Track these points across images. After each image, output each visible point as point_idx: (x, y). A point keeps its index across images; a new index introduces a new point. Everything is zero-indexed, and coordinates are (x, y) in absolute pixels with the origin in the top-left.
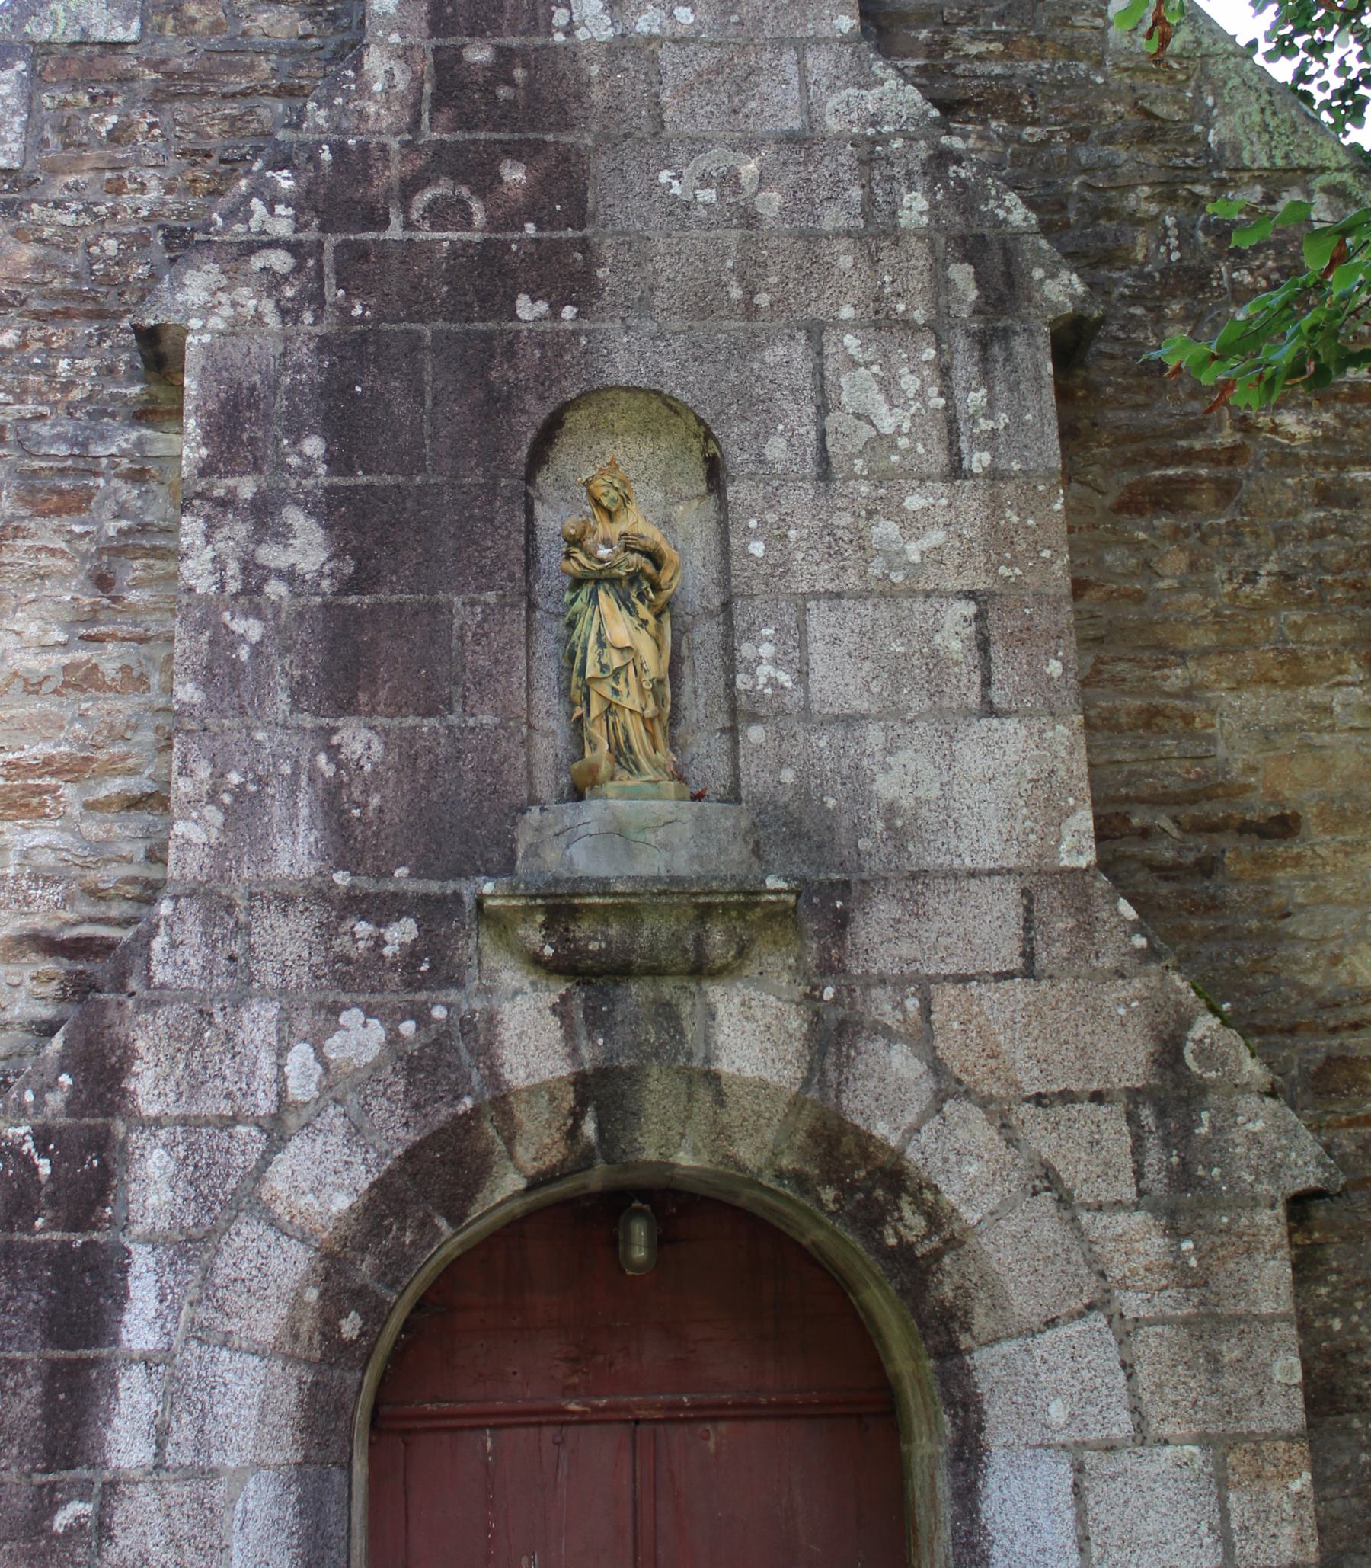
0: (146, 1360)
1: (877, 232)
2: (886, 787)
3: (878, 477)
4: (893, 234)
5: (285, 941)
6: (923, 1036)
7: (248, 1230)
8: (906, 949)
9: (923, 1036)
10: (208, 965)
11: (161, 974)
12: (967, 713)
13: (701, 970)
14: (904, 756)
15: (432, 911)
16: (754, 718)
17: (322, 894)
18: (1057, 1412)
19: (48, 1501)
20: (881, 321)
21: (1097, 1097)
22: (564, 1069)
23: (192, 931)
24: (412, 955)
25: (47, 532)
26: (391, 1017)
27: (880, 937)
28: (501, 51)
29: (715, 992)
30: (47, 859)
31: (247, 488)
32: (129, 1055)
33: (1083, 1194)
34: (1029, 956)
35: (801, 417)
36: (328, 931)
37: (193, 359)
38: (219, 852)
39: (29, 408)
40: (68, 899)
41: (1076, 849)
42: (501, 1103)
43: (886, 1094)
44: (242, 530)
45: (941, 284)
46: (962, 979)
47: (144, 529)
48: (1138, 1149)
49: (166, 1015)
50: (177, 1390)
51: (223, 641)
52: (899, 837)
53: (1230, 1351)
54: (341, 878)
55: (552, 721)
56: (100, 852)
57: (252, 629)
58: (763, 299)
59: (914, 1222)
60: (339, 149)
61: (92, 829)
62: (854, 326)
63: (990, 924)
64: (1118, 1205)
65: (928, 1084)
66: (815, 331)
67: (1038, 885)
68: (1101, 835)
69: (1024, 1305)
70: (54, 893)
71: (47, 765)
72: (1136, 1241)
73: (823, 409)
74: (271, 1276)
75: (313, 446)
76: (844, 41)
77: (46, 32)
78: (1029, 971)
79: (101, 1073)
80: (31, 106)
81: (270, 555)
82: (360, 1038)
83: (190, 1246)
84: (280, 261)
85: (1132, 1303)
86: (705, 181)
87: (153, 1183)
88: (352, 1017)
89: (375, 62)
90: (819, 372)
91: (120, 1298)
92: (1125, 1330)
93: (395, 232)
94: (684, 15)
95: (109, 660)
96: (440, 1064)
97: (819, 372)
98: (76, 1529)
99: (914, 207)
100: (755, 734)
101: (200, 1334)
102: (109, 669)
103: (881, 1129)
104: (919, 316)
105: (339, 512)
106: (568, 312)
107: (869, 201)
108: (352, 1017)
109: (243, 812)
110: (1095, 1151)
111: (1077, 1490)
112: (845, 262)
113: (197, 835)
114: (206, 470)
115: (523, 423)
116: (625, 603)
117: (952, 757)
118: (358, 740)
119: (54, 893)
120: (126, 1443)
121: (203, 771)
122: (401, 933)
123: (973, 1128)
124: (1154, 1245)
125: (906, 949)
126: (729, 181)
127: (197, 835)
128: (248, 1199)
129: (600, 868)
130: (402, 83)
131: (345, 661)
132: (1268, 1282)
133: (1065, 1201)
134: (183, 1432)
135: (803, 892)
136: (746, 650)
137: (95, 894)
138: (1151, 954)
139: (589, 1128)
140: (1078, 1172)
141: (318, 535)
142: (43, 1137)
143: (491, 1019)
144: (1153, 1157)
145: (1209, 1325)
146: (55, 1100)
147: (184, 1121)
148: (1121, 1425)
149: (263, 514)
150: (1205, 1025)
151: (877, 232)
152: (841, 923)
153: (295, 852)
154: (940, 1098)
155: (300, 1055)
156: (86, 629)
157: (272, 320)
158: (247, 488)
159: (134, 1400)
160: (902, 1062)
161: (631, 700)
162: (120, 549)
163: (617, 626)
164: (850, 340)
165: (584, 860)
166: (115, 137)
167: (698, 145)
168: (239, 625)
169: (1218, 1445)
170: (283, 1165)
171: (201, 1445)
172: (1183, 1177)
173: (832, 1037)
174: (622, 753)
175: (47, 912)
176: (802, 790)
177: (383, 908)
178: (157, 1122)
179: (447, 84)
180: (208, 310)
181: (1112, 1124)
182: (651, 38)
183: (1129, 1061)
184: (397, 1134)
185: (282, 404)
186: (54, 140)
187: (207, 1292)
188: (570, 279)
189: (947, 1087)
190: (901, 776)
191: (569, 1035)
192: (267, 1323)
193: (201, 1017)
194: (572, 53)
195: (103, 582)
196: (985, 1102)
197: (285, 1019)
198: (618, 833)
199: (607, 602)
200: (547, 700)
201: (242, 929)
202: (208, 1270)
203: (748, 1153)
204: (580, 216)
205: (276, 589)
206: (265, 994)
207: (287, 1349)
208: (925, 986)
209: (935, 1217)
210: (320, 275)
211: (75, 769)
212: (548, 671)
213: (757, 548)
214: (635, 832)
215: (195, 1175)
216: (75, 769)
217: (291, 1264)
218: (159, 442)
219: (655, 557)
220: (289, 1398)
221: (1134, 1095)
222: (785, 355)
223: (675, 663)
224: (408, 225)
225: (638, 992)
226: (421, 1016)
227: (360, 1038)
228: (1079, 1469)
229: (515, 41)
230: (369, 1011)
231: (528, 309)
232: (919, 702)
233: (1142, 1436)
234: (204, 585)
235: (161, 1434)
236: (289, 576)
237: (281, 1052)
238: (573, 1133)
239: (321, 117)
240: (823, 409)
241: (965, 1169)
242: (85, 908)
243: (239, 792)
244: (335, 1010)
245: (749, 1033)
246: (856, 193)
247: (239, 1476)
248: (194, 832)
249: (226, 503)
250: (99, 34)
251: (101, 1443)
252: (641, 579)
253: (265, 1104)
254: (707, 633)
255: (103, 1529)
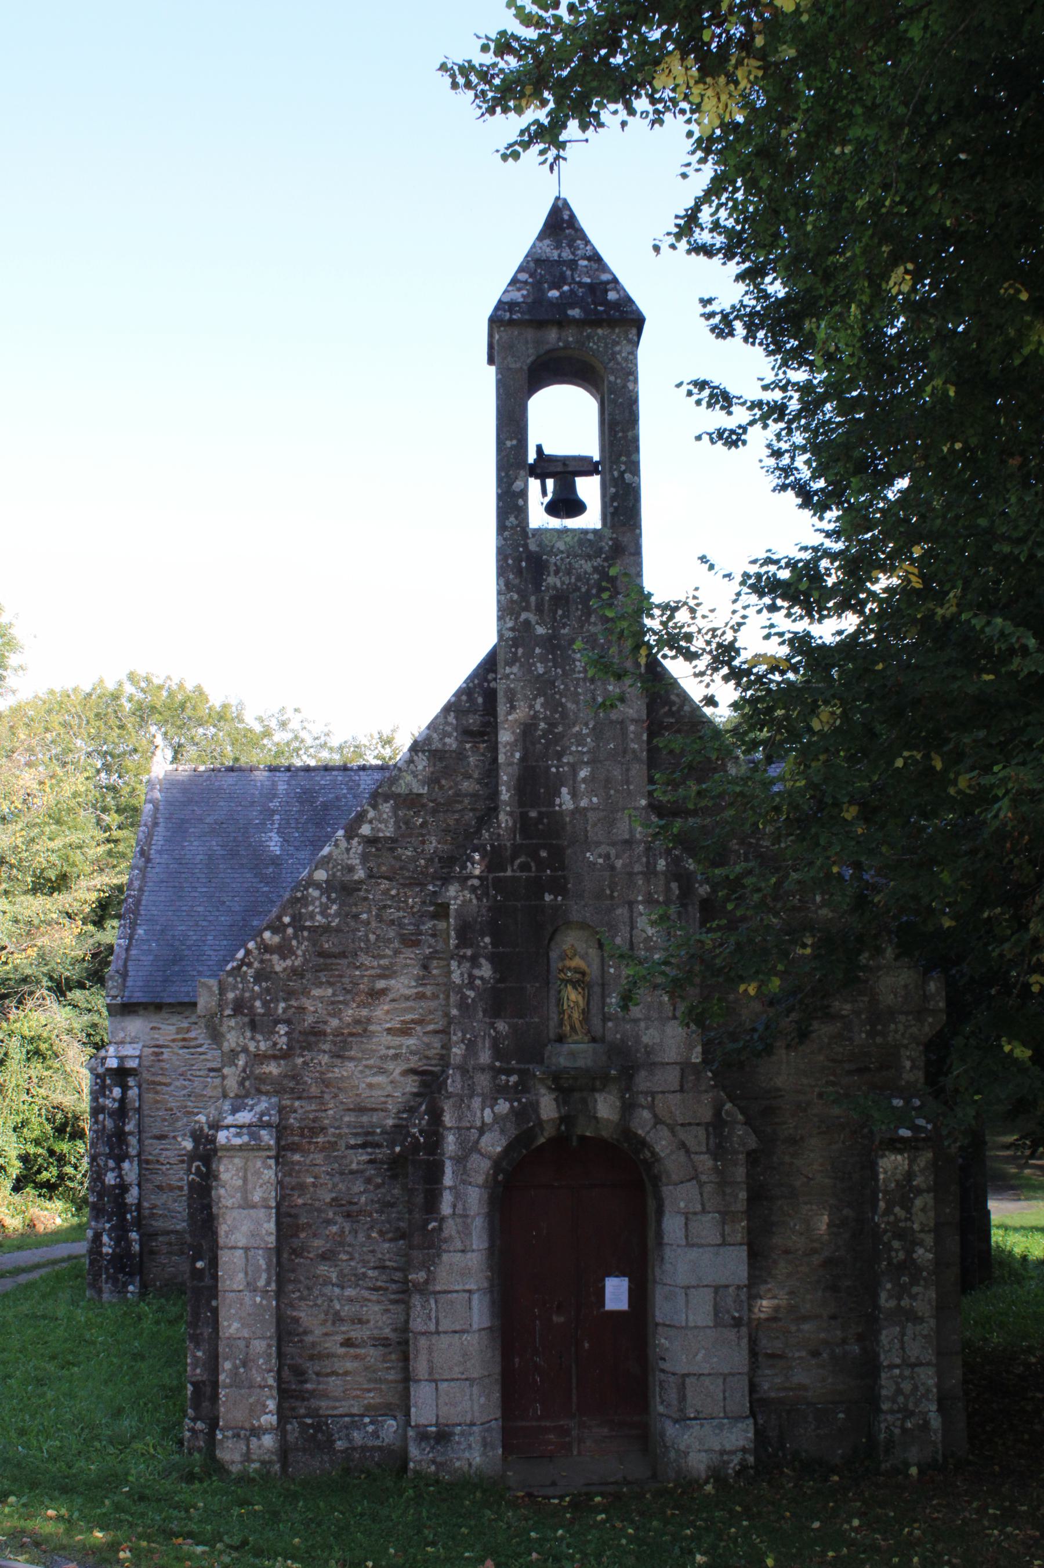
0: (450, 1188)
1: (650, 872)
2: (645, 1039)
3: (647, 949)
4: (655, 873)
5: (483, 1081)
6: (652, 1107)
7: (475, 1156)
8: (648, 1084)
9: (652, 1107)
10: (463, 1087)
11: (450, 1089)
12: (669, 1019)
13: (594, 1090)
14: (651, 1030)
15: (523, 1073)
16: (610, 1020)
17: (492, 1068)
18: (682, 1205)
19: (427, 1222)
20: (650, 901)
21: (698, 1124)
22: (556, 1115)
23: (458, 1078)
24: (516, 1084)
25: (408, 953)
26: (511, 1102)
27: (643, 1081)
28: (540, 813)
29: (597, 1095)
30: (414, 1048)
31: (469, 952)
32: (443, 1111)
33: (693, 1149)
34: (682, 1086)
35: (625, 931)
36: (494, 1078)
37: (452, 913)
38: (464, 1057)
39: (401, 914)
40: (420, 1059)
41: (696, 1058)
42: (540, 1123)
43: (642, 1121)
44: (468, 965)
45: (668, 890)
46: (663, 1092)
47: (436, 952)
48: (708, 1138)
49: (452, 1100)
50: (458, 1196)
51: (464, 997)
52: (648, 1053)
53: (728, 1190)
54: (497, 1064)
55: (554, 1016)
56: (428, 1046)
57: (471, 994)
58: (616, 894)
59: (648, 1154)
60: (492, 846)
61: (426, 1039)
62: (641, 902)
63: (671, 1078)
64: (701, 1153)
65: (652, 1122)
66: (631, 904)
67: (685, 1066)
68: (704, 1053)
69: (674, 1177)
70: (416, 1058)
71: (413, 1021)
72: (705, 1162)
73: (632, 929)
74: (480, 1167)
75: (487, 940)
76: (643, 808)
77: (399, 791)
78: (682, 1090)
79: (436, 1115)
80: (396, 815)
81: (477, 972)
82: (503, 1107)
83: (460, 1161)
84: (476, 882)
85: (704, 1178)
86: (600, 856)
87: (451, 1143)
88: (501, 1101)
89: (502, 817)
90: (631, 917)
91: (443, 1173)
92: (701, 1185)
93: (509, 873)
94: (595, 800)
95: (428, 990)
96: (525, 1114)
97: (631, 917)
98: (434, 1229)
99: (661, 864)
100: (610, 1024)
101: (463, 1182)
102: (429, 994)
103: (640, 1132)
104: (661, 899)
105: (493, 959)
106: (560, 898)
107: (648, 862)
108: (501, 1101)
109: (471, 1047)
110: (695, 1139)
111: (686, 1224)
112: (640, 882)
113: (458, 1052)
114: (457, 947)
115: (544, 928)
116: (575, 988)
117: (664, 1031)
118: (502, 1026)
119: (416, 1058)
120: (446, 1209)
121: (460, 1034)
122: (514, 1079)
123: (665, 1132)
124: (710, 1163)
125: (648, 1084)
126: (607, 857)
127: (458, 1052)
128: (475, 1148)
129: (568, 1064)
130: (510, 824)
131: (498, 1001)
132: (740, 1173)
133: (688, 1152)
134: (460, 1206)
135: (624, 1065)
136: (608, 1000)
137: (427, 1058)
138: (714, 1087)
139: (563, 1128)
140: (691, 1142)
141: (489, 966)
142: (421, 1132)
143: (538, 1102)
144: (711, 1141)
145: (723, 1181)
146: (424, 1122)
147: (458, 1128)
148: (698, 1208)
149: (474, 961)
150: (728, 1106)
151: (650, 872)
152: (631, 1077)
153: (485, 1057)
154: (656, 1124)
155: (487, 1111)
156: (421, 981)
157: (475, 901)
158: (469, 952)
159: (447, 1198)
160: (646, 1114)
161: (576, 1015)
162: (429, 958)
163: (573, 996)
164: (641, 907)
165: (563, 1062)
166: (422, 825)
167: (598, 844)
168: (468, 993)
169: (724, 1214)
170: (484, 1140)
171: (465, 1209)
172: (719, 1146)
173: (628, 1108)
174: (573, 1028)
175: (414, 1062)
176: (622, 1040)
177: (509, 1072)
178: (451, 1128)
179: (524, 825)
180: (455, 898)
181: (701, 1132)
182: (585, 809)
183: (706, 1114)
184: (513, 1132)
185: (478, 927)
186: (404, 827)
187: (465, 1172)
188: (559, 887)
189: (658, 1121)
190: (649, 1036)
191: (558, 1107)
192: (480, 1179)
193: (461, 1101)
194: (561, 813)
195: (425, 967)
196: (667, 1125)
197: (483, 1102)
198: (573, 1055)
199: (569, 987)
200: (553, 1009)
201: (472, 1078)
202: (465, 1166)
203: (605, 1134)
204: (563, 868)
205: (478, 982)
206: (478, 1095)
207: (485, 1186)
208: (653, 1094)
209: (654, 1154)
210: (487, 887)
211: (420, 1022)
212: (553, 1001)
213: (612, 970)
214: (576, 1053)
215: (461, 1143)
216: (420, 1022)
217: (486, 1165)
218: (442, 925)
219: (584, 974)
220: (486, 1196)
221: (708, 1125)
222: (621, 912)
223: (588, 1004)
224: (513, 871)
225: (577, 1095)
226: (519, 1101)
227: (503, 1107)
228: (687, 1219)
229: (544, 809)
230: (505, 1100)
231: (548, 898)
232: (654, 1015)
233: (704, 1211)
234: (458, 981)
235: (454, 1206)
236: (481, 978)
237: (482, 1110)
238: (559, 1129)
239: (487, 835)
240: (632, 929)
241: (662, 1143)
242: (425, 1061)
243: (470, 1040)
244: (496, 1099)
245: (606, 1107)
246: (644, 860)
247: (474, 1218)
248: (458, 1051)
249: (464, 957)
250: (415, 791)
251: (439, 1209)
252: (580, 981)
253: (478, 1124)
254: (597, 989)
255: (440, 1229)
